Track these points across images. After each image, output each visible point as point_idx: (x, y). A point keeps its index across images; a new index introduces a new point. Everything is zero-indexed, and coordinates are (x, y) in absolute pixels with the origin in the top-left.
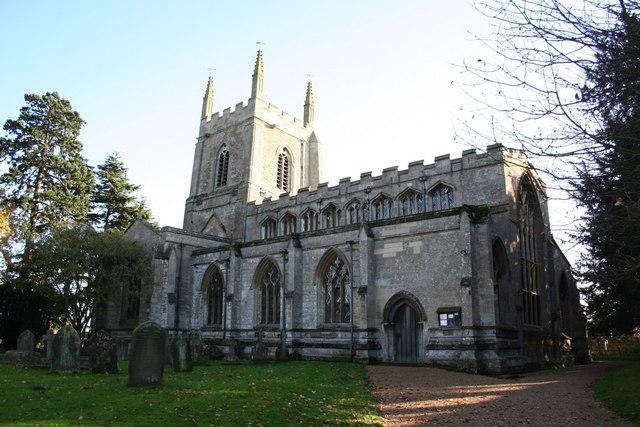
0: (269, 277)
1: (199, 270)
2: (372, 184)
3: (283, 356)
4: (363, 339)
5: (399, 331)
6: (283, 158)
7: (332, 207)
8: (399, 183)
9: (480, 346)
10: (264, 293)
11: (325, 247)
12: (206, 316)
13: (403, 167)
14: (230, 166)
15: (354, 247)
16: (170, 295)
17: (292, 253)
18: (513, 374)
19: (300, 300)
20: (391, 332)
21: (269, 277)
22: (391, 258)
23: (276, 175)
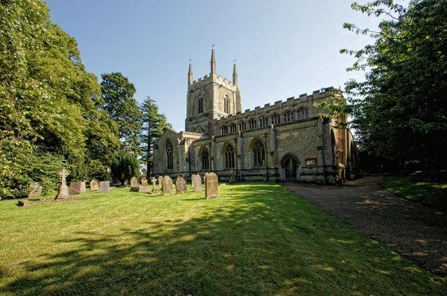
4: (272, 172)
13: (284, 100)
16: (187, 159)
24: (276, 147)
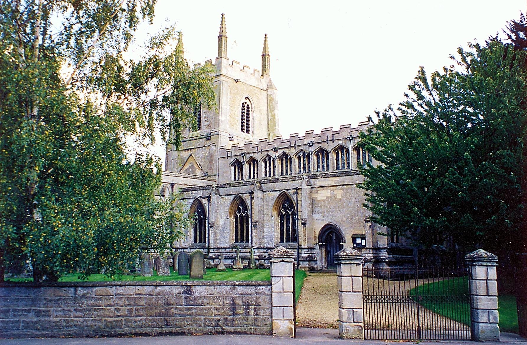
0: (240, 208)
1: (186, 203)
2: (313, 140)
3: (252, 266)
5: (329, 249)
6: (246, 105)
7: (285, 155)
8: (333, 140)
9: (377, 261)
10: (237, 221)
11: (280, 191)
12: (193, 238)
13: (336, 128)
14: (203, 115)
15: (299, 191)
17: (258, 194)
18: (422, 276)
19: (263, 226)
20: (323, 250)
21: (240, 208)
22: (322, 200)
23: (241, 111)
24: (313, 211)
